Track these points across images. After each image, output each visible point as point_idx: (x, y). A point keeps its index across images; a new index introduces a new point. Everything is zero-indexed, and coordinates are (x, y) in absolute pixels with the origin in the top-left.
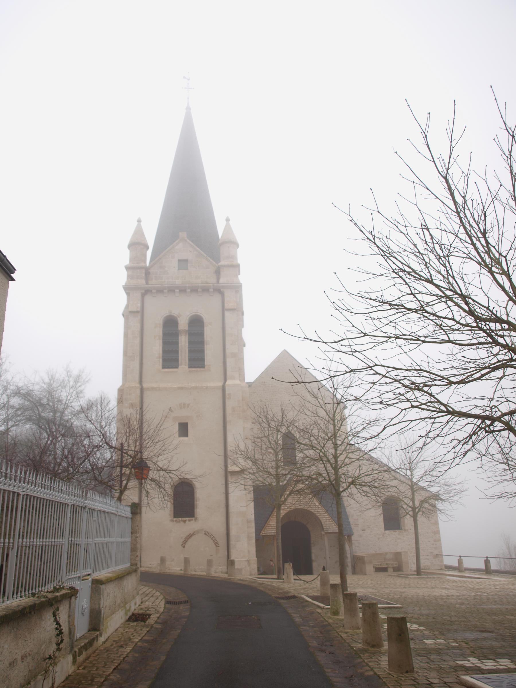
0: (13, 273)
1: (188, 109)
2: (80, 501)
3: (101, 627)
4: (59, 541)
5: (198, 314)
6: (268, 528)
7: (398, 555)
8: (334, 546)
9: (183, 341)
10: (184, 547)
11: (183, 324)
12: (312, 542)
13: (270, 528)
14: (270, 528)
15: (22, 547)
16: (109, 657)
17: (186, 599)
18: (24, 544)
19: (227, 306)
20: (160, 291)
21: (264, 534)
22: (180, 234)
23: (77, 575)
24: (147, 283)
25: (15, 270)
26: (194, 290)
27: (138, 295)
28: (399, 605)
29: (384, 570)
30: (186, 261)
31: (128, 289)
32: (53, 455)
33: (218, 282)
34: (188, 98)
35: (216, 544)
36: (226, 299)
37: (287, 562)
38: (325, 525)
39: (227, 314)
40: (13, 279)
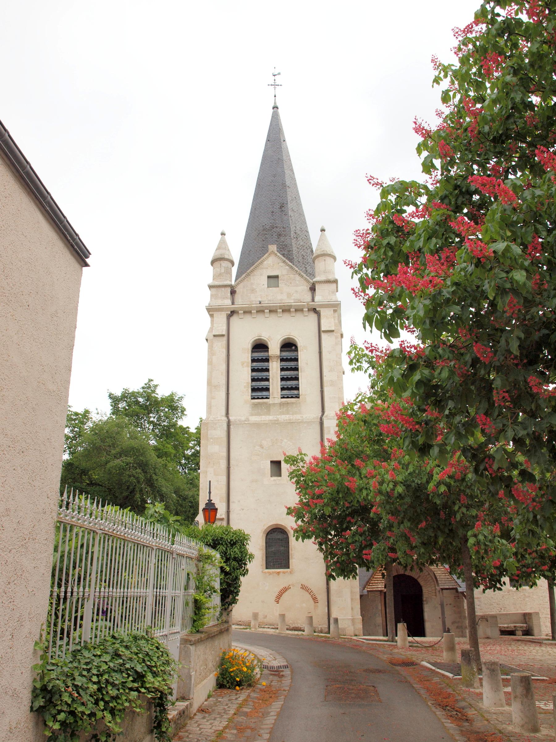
0: (87, 257)
1: (275, 107)
2: (166, 544)
3: (191, 696)
4: (141, 591)
5: (262, 338)
6: (373, 582)
7: (526, 617)
8: (450, 604)
9: (275, 367)
10: (278, 602)
11: (274, 350)
12: (424, 599)
13: (376, 582)
14: (376, 582)
15: (99, 598)
16: (202, 732)
17: (286, 664)
18: (102, 594)
19: (323, 328)
20: (247, 312)
22: (270, 247)
23: (164, 634)
24: (233, 303)
25: (90, 254)
26: (286, 310)
27: (221, 318)
28: (545, 678)
29: (512, 633)
30: (277, 277)
31: (211, 311)
32: (543, 19)
33: (313, 300)
34: (275, 96)
35: (315, 599)
36: (323, 321)
37: (400, 622)
38: (440, 579)
39: (323, 336)
40: (87, 265)
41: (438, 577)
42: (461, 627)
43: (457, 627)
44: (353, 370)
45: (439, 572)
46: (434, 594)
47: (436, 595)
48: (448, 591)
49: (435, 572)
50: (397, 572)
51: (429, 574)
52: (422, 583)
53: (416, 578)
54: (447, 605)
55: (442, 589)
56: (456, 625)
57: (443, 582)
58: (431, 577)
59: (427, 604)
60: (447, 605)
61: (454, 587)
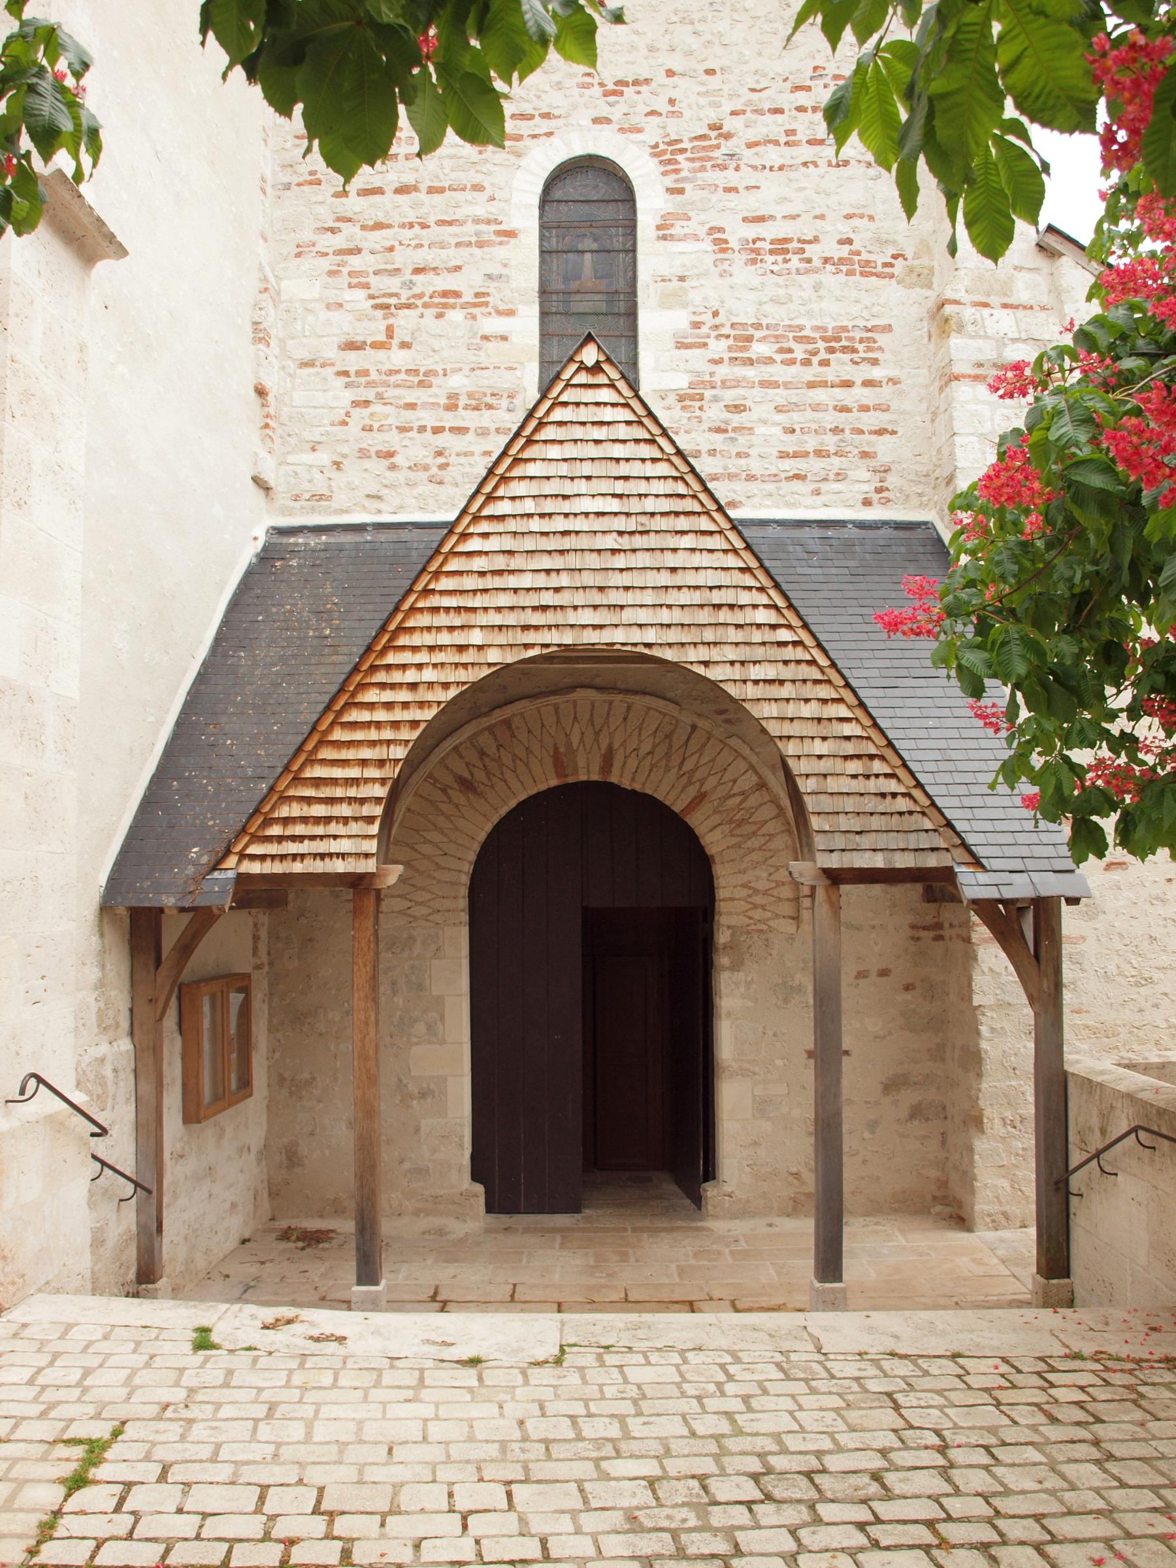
6: (296, 810)
8: (884, 973)
12: (722, 937)
13: (319, 810)
14: (319, 810)
21: (255, 868)
38: (827, 803)
41: (810, 803)
42: (942, 1111)
43: (916, 1112)
44: (659, 238)
45: (820, 748)
46: (787, 909)
47: (796, 918)
48: (877, 889)
49: (796, 767)
50: (559, 764)
51: (762, 785)
52: (714, 841)
53: (677, 808)
54: (861, 975)
55: (835, 877)
56: (909, 1097)
57: (844, 823)
58: (775, 801)
59: (735, 967)
60: (861, 975)
61: (932, 861)
